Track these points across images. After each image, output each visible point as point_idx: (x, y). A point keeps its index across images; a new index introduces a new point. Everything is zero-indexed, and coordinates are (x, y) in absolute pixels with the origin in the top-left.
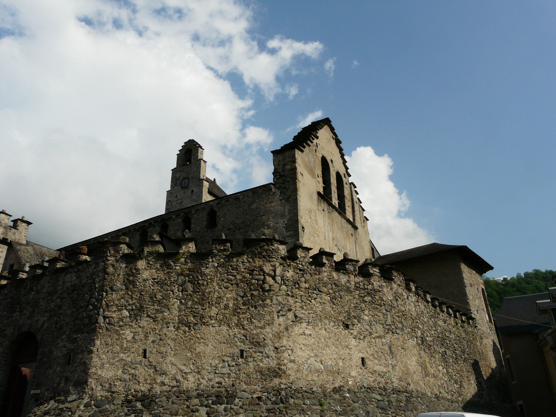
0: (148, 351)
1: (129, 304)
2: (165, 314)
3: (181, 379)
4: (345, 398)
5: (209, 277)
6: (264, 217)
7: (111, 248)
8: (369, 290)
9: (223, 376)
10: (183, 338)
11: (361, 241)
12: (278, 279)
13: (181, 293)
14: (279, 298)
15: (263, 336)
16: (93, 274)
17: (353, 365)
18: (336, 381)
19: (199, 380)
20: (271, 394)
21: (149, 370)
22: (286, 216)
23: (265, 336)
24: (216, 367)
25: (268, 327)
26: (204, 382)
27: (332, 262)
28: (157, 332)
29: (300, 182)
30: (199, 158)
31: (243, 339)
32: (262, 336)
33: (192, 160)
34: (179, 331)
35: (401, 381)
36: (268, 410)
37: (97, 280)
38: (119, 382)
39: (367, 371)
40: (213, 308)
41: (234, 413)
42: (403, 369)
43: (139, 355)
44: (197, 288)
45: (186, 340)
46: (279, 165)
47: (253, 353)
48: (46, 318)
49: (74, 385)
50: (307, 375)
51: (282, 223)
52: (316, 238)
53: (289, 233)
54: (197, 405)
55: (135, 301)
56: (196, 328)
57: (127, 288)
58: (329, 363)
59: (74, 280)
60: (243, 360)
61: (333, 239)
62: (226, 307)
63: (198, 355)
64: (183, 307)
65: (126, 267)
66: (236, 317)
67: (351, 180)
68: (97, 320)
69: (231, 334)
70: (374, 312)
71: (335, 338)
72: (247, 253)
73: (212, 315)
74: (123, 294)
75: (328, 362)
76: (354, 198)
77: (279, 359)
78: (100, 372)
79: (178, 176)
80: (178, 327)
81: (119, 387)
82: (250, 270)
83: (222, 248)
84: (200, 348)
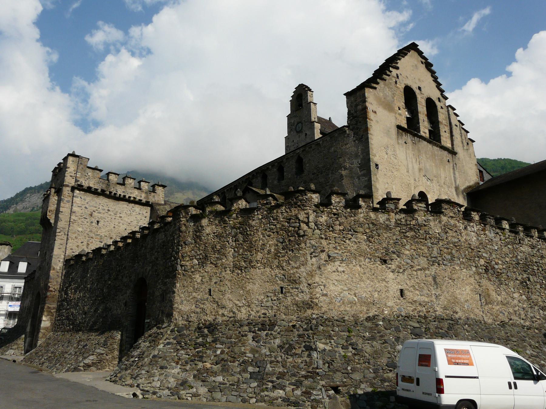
0: (212, 290)
1: (198, 255)
2: (223, 261)
3: (236, 312)
4: (377, 325)
5: (255, 228)
6: (340, 159)
7: (182, 211)
8: (412, 226)
9: (267, 308)
10: (237, 279)
11: (463, 166)
12: (312, 225)
13: (234, 243)
14: (311, 241)
15: (298, 275)
16: (173, 232)
17: (390, 296)
18: (370, 311)
19: (249, 312)
20: (304, 323)
21: (213, 305)
22: (360, 156)
23: (300, 274)
24: (262, 302)
25: (302, 267)
26: (253, 313)
27: (369, 203)
28: (218, 275)
29: (372, 120)
30: (309, 101)
31: (283, 278)
32: (297, 275)
33: (303, 105)
34: (234, 273)
35: (446, 309)
36: (299, 336)
37: (175, 237)
38: (194, 314)
39: (405, 301)
40: (259, 254)
41: (272, 338)
42: (449, 298)
43: (206, 294)
44: (246, 238)
45: (239, 281)
46: (352, 107)
47: (291, 289)
48: (150, 268)
49: (166, 317)
50: (339, 307)
51: (356, 163)
52: (396, 173)
53: (362, 172)
54: (246, 331)
55: (201, 252)
56: (246, 270)
57: (196, 242)
58: (364, 296)
59: (163, 238)
60: (283, 295)
61: (420, 170)
62: (269, 252)
63: (248, 292)
64: (236, 254)
65: (194, 225)
66: (277, 260)
67: (448, 103)
68: (176, 268)
69: (273, 274)
70: (417, 246)
71: (370, 273)
72: (285, 204)
73: (258, 259)
74: (193, 247)
75: (362, 295)
76: (452, 121)
77: (311, 294)
78: (180, 307)
79: (292, 122)
80: (233, 270)
81: (194, 318)
82: (287, 219)
83: (265, 202)
84: (250, 287)
